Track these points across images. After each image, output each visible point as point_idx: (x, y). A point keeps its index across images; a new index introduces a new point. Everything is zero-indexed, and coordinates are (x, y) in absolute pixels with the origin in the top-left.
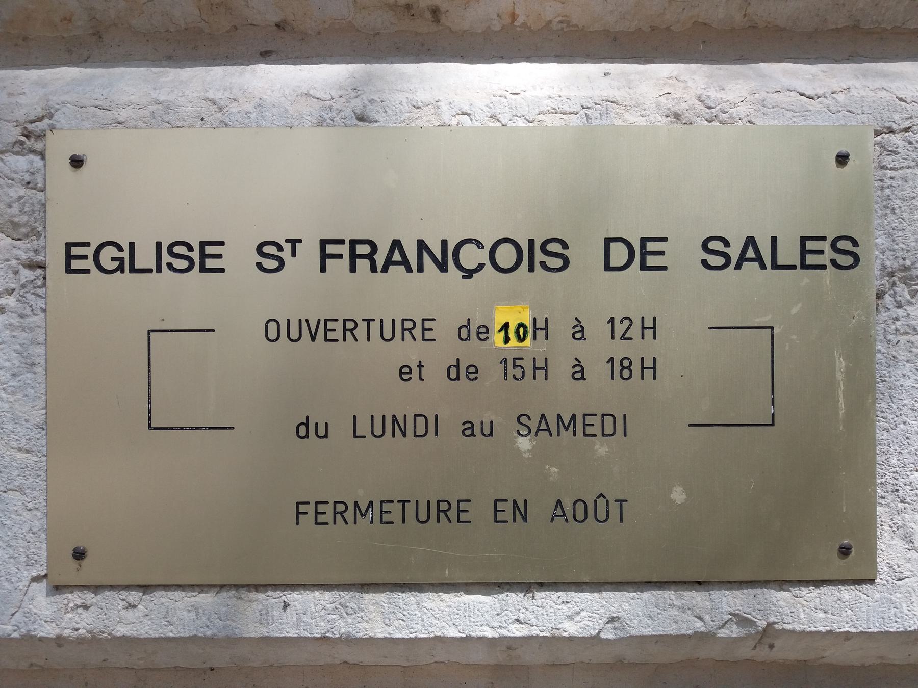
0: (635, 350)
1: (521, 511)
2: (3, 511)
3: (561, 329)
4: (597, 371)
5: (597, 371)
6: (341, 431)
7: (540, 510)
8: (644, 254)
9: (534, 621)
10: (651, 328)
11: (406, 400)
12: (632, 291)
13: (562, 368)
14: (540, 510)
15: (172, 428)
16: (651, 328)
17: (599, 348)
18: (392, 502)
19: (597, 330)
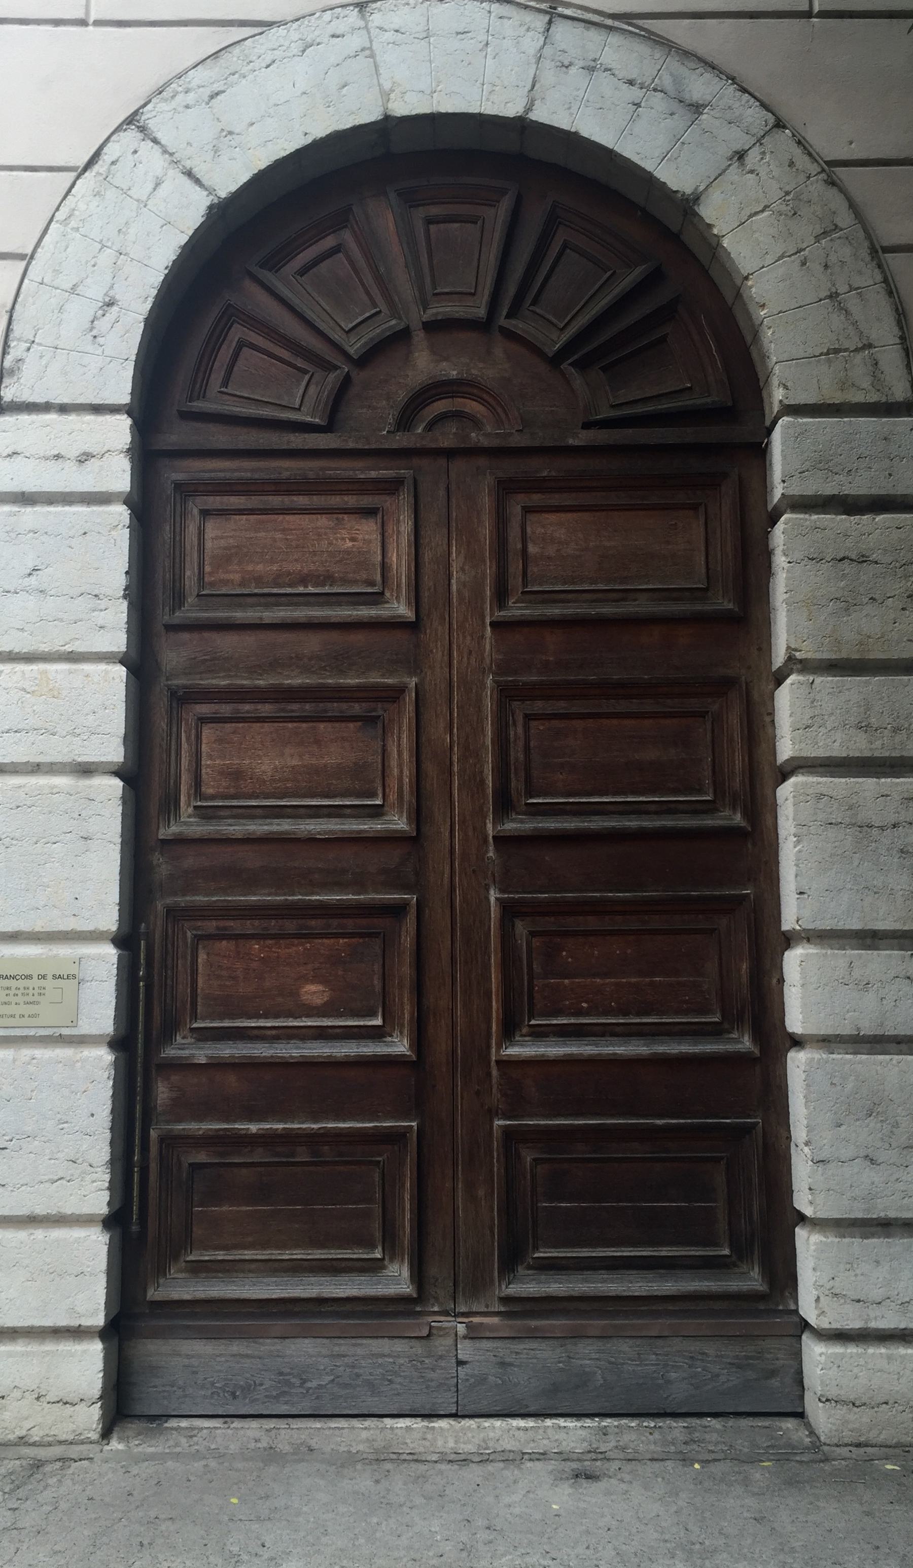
0: (42, 991)
1: (23, 1016)
2: (911, 1183)
3: (31, 988)
4: (36, 995)
5: (36, 995)
6: (50, 977)
7: (26, 1016)
8: (44, 977)
9: (517, 1433)
10: (44, 988)
11: (7, 999)
12: (42, 983)
13: (31, 994)
14: (26, 1016)
15: (57, 22)
16: (44, 988)
17: (36, 991)
18: (29, 1016)
19: (36, 988)
